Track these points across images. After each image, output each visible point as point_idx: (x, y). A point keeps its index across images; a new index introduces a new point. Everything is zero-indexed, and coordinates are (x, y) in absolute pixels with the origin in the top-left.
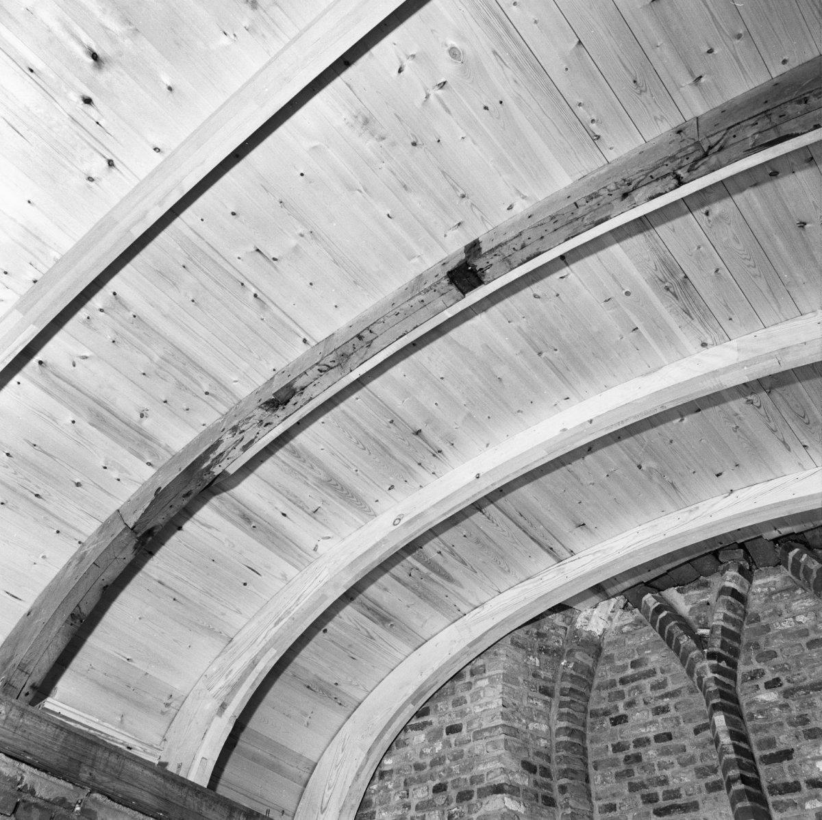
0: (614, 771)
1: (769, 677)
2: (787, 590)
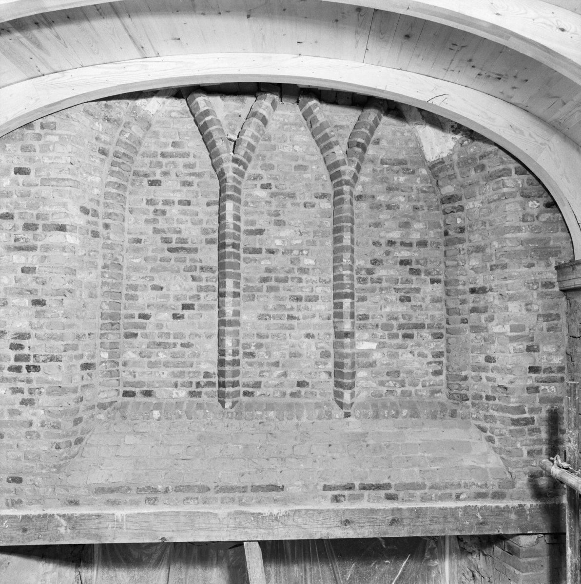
0: (144, 217)
1: (265, 181)
2: (295, 124)
